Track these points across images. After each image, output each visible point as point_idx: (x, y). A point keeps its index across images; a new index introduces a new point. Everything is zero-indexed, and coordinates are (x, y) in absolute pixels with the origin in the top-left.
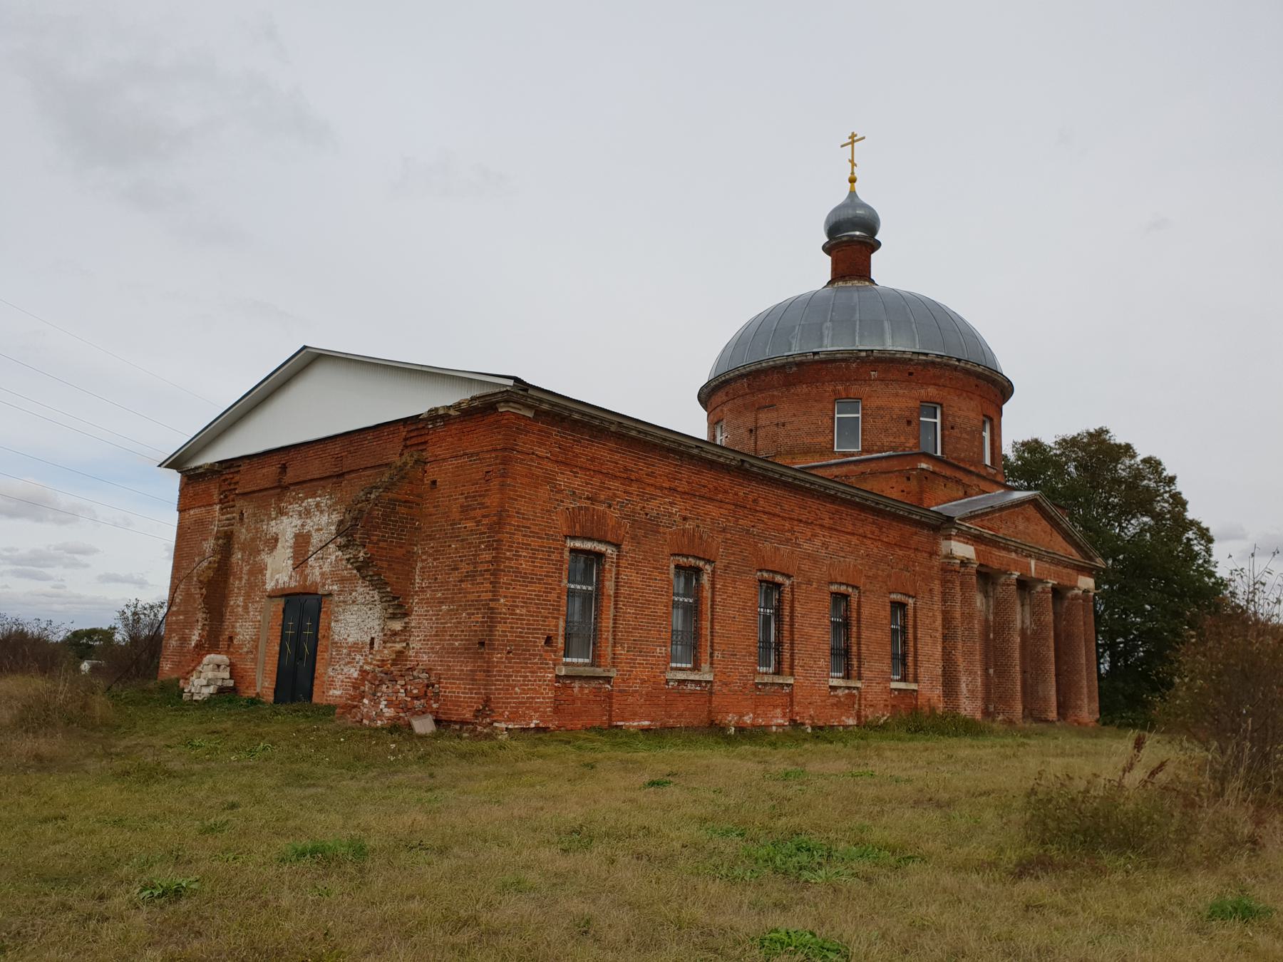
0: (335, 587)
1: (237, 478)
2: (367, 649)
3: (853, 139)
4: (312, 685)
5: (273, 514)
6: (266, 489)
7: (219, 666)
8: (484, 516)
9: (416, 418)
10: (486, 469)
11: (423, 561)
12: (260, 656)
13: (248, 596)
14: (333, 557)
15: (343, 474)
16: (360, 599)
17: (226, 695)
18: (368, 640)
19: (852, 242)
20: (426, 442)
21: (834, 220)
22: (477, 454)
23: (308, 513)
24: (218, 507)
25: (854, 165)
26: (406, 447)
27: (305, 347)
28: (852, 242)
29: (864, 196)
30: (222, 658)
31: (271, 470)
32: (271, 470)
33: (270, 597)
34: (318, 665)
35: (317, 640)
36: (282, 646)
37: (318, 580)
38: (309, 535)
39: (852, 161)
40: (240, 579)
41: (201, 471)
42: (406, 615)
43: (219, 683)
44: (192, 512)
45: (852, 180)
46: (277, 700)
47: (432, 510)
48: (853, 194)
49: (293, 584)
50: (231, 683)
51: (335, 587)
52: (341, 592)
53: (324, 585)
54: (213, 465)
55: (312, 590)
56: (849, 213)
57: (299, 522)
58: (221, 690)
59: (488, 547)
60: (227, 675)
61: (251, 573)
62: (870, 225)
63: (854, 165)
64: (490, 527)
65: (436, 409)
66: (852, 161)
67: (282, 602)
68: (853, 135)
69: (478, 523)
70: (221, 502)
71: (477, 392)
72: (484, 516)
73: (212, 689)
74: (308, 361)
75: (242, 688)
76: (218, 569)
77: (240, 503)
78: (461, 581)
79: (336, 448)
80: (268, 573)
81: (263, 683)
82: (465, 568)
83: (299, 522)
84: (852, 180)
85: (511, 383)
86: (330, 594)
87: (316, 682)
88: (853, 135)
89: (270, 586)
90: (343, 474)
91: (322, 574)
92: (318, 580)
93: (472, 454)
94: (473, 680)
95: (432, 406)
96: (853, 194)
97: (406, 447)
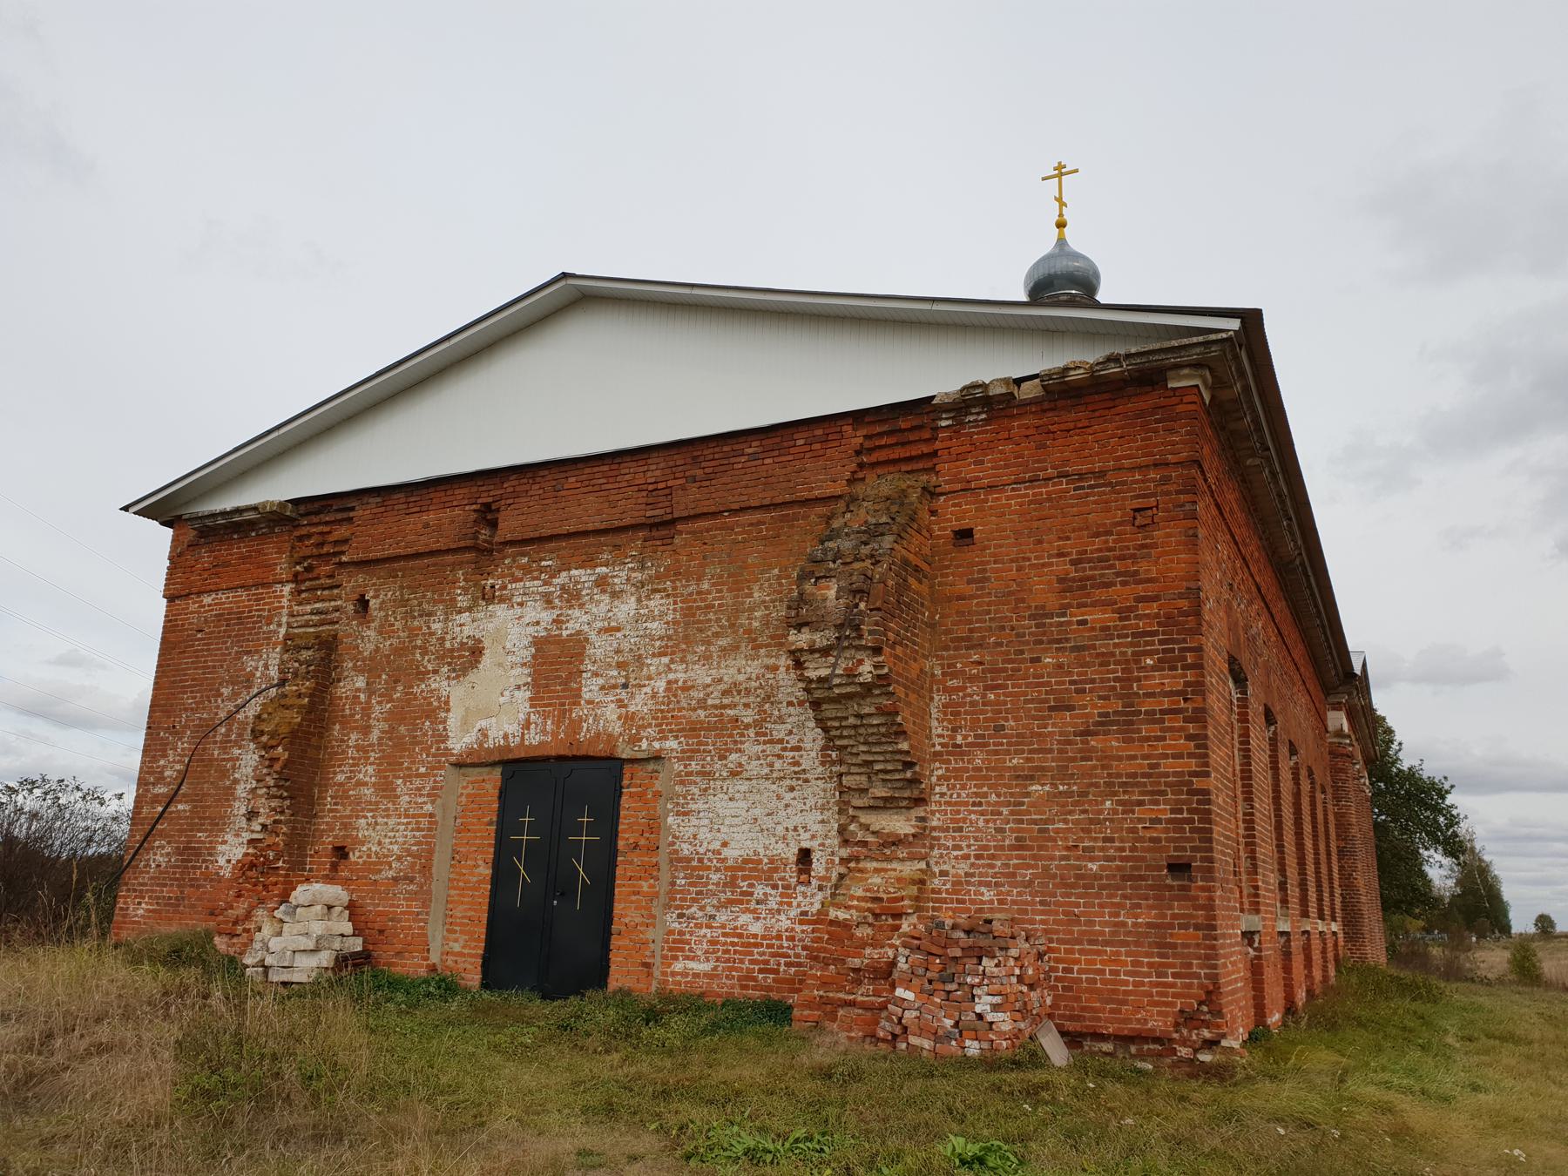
1: (341, 532)
2: (791, 875)
3: (1060, 171)
4: (606, 948)
5: (463, 601)
6: (438, 552)
7: (330, 907)
8: (1139, 599)
9: (923, 405)
10: (1137, 503)
11: (947, 690)
12: (438, 888)
13: (391, 764)
14: (661, 685)
15: (673, 522)
16: (754, 768)
17: (358, 969)
18: (791, 853)
20: (935, 454)
21: (1042, 272)
22: (1102, 474)
23: (572, 596)
24: (287, 588)
25: (1062, 204)
26: (861, 466)
27: (565, 275)
29: (1076, 242)
30: (335, 893)
31: (452, 519)
32: (452, 519)
33: (459, 765)
34: (618, 908)
35: (614, 852)
36: (497, 865)
37: (616, 728)
38: (578, 643)
39: (1059, 199)
40: (366, 730)
41: (251, 516)
42: (920, 801)
43: (337, 946)
44: (207, 600)
45: (1061, 225)
46: (485, 985)
47: (962, 587)
48: (1061, 242)
49: (533, 738)
50: (357, 945)
51: (672, 744)
52: (688, 755)
55: (600, 749)
56: (1062, 266)
57: (546, 617)
58: (342, 961)
59: (1167, 662)
60: (347, 928)
61: (395, 717)
63: (1062, 204)
64: (1168, 621)
65: (984, 386)
66: (1059, 199)
68: (1060, 167)
69: (1124, 613)
70: (296, 578)
72: (1139, 599)
73: (326, 958)
74: (571, 300)
75: (384, 954)
76: (311, 708)
77: (353, 583)
79: (654, 470)
80: (453, 720)
81: (451, 939)
82: (1092, 707)
83: (546, 617)
84: (1061, 225)
85: (1234, 324)
86: (657, 758)
87: (615, 942)
88: (1060, 167)
89: (459, 742)
90: (673, 522)
91: (628, 719)
92: (616, 728)
96: (1061, 242)
97: (861, 466)
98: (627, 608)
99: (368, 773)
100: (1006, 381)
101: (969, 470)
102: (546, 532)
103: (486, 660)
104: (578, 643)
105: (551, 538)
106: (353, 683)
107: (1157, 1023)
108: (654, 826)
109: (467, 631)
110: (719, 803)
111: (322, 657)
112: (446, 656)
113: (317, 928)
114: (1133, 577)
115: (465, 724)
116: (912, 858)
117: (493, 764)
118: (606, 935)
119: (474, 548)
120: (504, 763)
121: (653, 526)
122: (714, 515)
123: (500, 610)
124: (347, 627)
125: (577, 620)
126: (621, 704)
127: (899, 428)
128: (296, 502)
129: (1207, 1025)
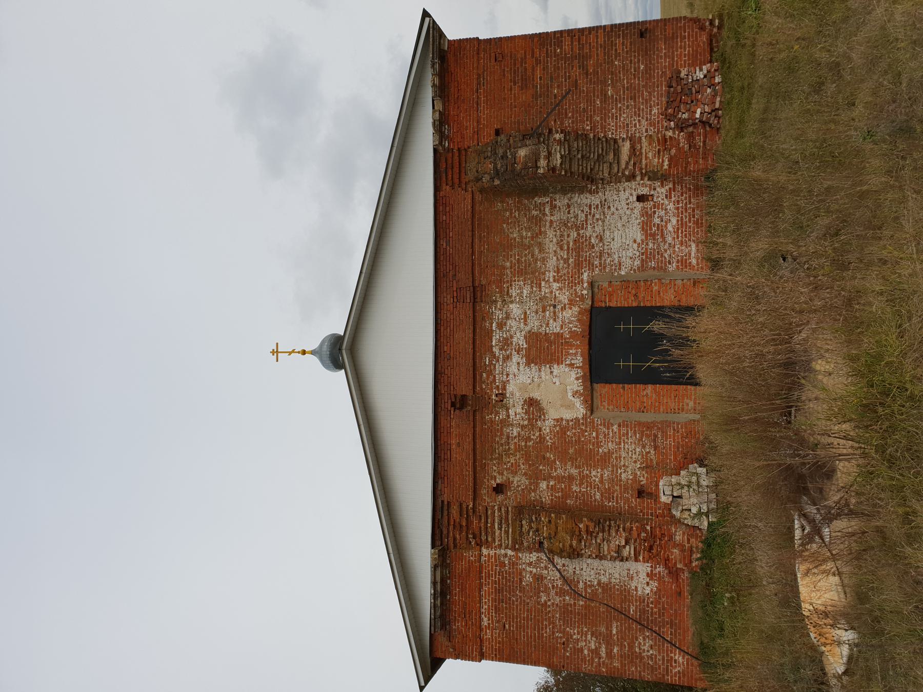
3: (276, 352)
8: (533, 56)
12: (660, 417)
18: (639, 205)
22: (479, 75)
23: (506, 343)
24: (485, 551)
29: (314, 345)
33: (592, 412)
39: (290, 353)
45: (304, 352)
48: (313, 353)
49: (579, 361)
52: (591, 266)
57: (515, 358)
63: (293, 351)
67: (595, 385)
68: (273, 352)
69: (538, 62)
71: (428, 93)
78: (587, 74)
84: (304, 352)
88: (273, 352)
93: (479, 84)
94: (673, 38)
96: (313, 353)
110: (615, 246)
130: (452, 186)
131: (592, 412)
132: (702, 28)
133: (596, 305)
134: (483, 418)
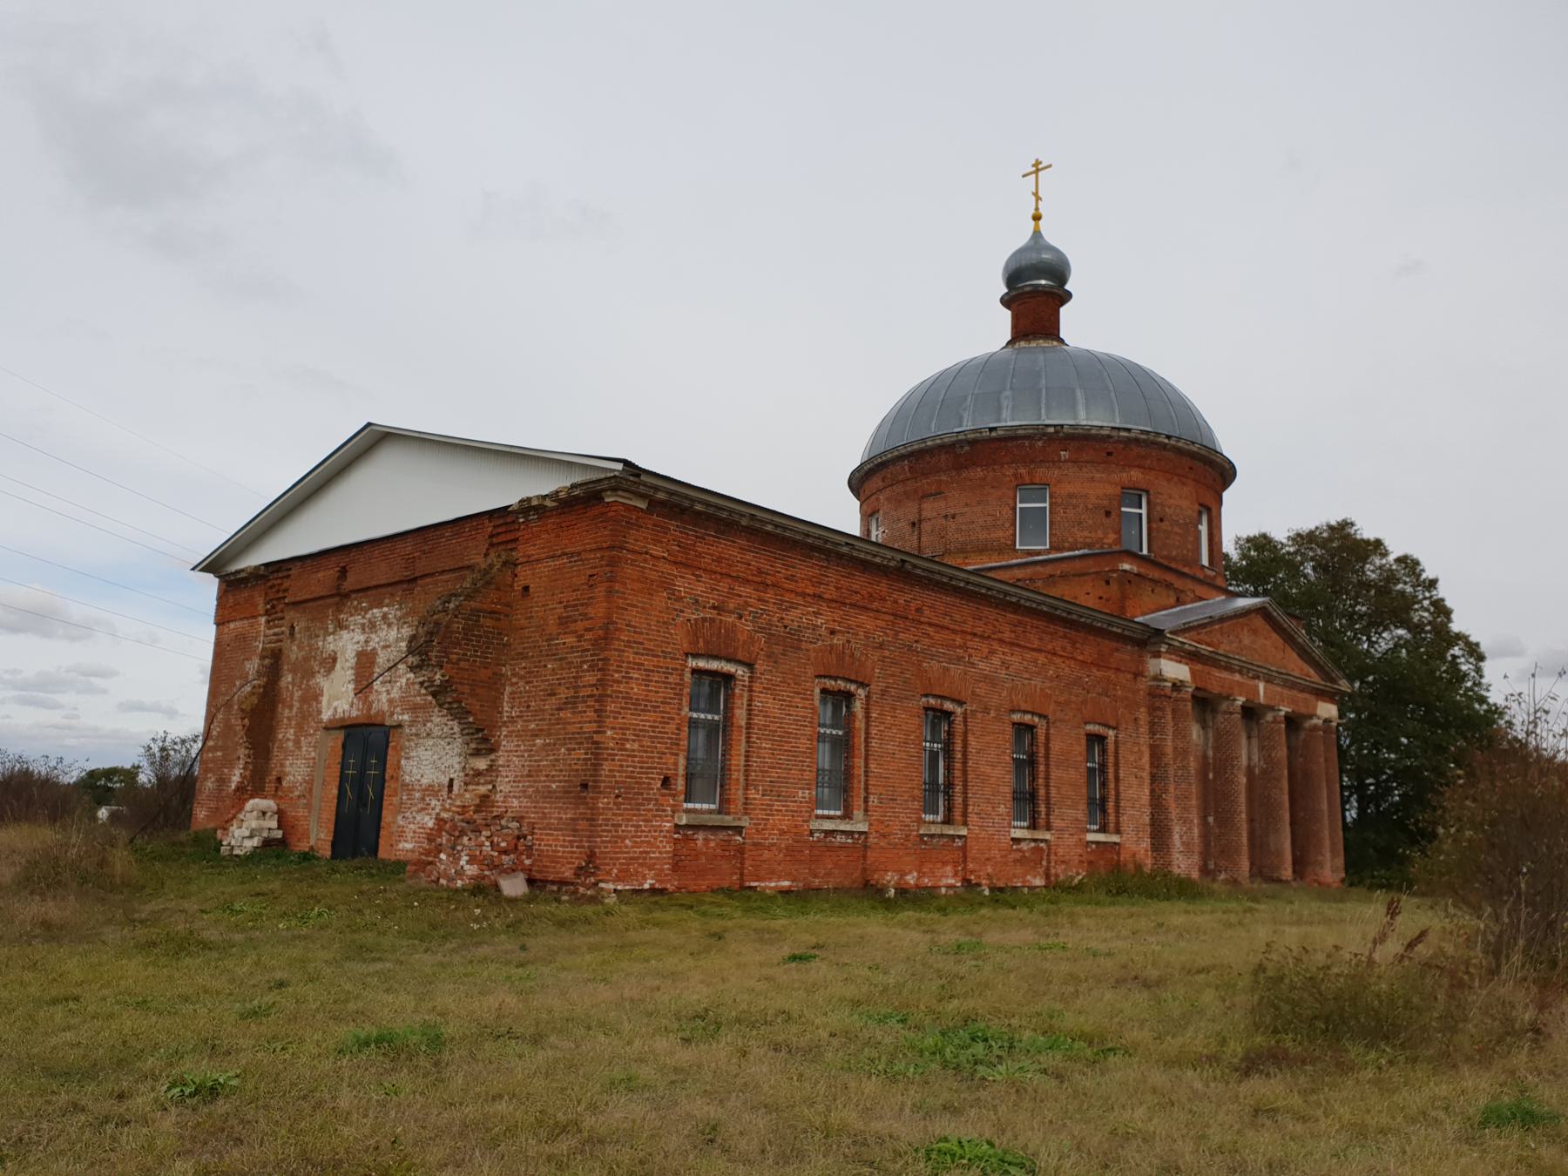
0: (406, 717)
1: (286, 584)
3: (1037, 168)
4: (378, 837)
7: (264, 813)
10: (589, 572)
13: (300, 728)
14: (404, 681)
15: (415, 579)
18: (446, 781)
19: (1036, 294)
21: (1014, 266)
22: (579, 554)
24: (263, 620)
25: (1038, 199)
26: (492, 545)
27: (369, 424)
28: (1036, 294)
29: (1051, 237)
30: (269, 804)
32: (325, 577)
33: (326, 728)
34: (384, 812)
35: (384, 780)
37: (386, 708)
38: (374, 653)
39: (1036, 194)
40: (291, 707)
41: (243, 575)
42: (492, 750)
43: (265, 834)
44: (232, 626)
45: (1037, 218)
48: (1037, 234)
49: (354, 713)
50: (279, 834)
51: (406, 717)
52: (413, 723)
53: (392, 714)
54: (257, 568)
55: (378, 720)
56: (1033, 258)
57: (362, 638)
60: (274, 824)
61: (303, 700)
62: (1058, 272)
63: (1038, 199)
66: (1036, 194)
68: (1037, 163)
70: (267, 613)
71: (578, 478)
73: (255, 842)
74: (372, 441)
77: (290, 615)
78: (559, 709)
79: (407, 547)
80: (325, 700)
81: (318, 834)
82: (564, 692)
83: (362, 638)
84: (1037, 218)
85: (620, 466)
87: (382, 832)
89: (326, 716)
90: (415, 579)
92: (386, 708)
95: (524, 495)
96: (1037, 234)
97: (492, 545)
98: (393, 634)
99: (291, 733)
100: (537, 497)
101: (532, 551)
102: (365, 585)
103: (338, 666)
104: (374, 653)
105: (368, 588)
106: (287, 679)
107: (568, 874)
108: (399, 767)
109: (332, 647)
110: (421, 751)
111: (274, 661)
112: (323, 662)
113: (254, 824)
114: (586, 617)
115: (329, 703)
116: (486, 783)
117: (341, 728)
118: (378, 828)
119: (338, 595)
120: (341, 728)
121: (409, 581)
122: (432, 575)
123: (344, 633)
124: (286, 644)
125: (375, 641)
126: (388, 692)
127: (500, 524)
128: (267, 565)
129: (593, 874)
130: (491, 536)
131: (326, 728)
132: (580, 871)
133: (828, 722)
134: (329, 606)
